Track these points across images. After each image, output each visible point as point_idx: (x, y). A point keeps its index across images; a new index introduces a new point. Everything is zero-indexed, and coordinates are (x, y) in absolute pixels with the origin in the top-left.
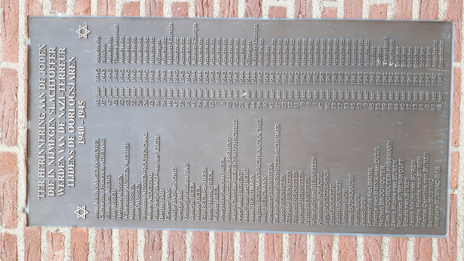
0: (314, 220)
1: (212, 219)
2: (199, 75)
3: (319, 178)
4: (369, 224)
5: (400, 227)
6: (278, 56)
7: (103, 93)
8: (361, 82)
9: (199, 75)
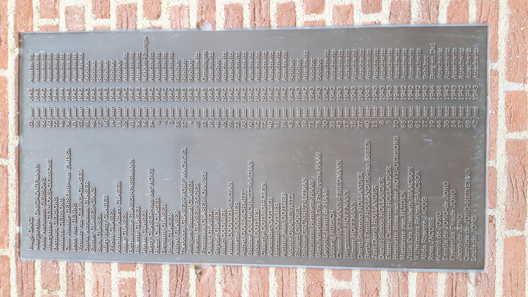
0: (418, 255)
1: (279, 254)
2: (61, 93)
3: (283, 204)
4: (473, 258)
5: (426, 258)
6: (68, 72)
7: (36, 114)
8: (376, 97)
9: (61, 93)
